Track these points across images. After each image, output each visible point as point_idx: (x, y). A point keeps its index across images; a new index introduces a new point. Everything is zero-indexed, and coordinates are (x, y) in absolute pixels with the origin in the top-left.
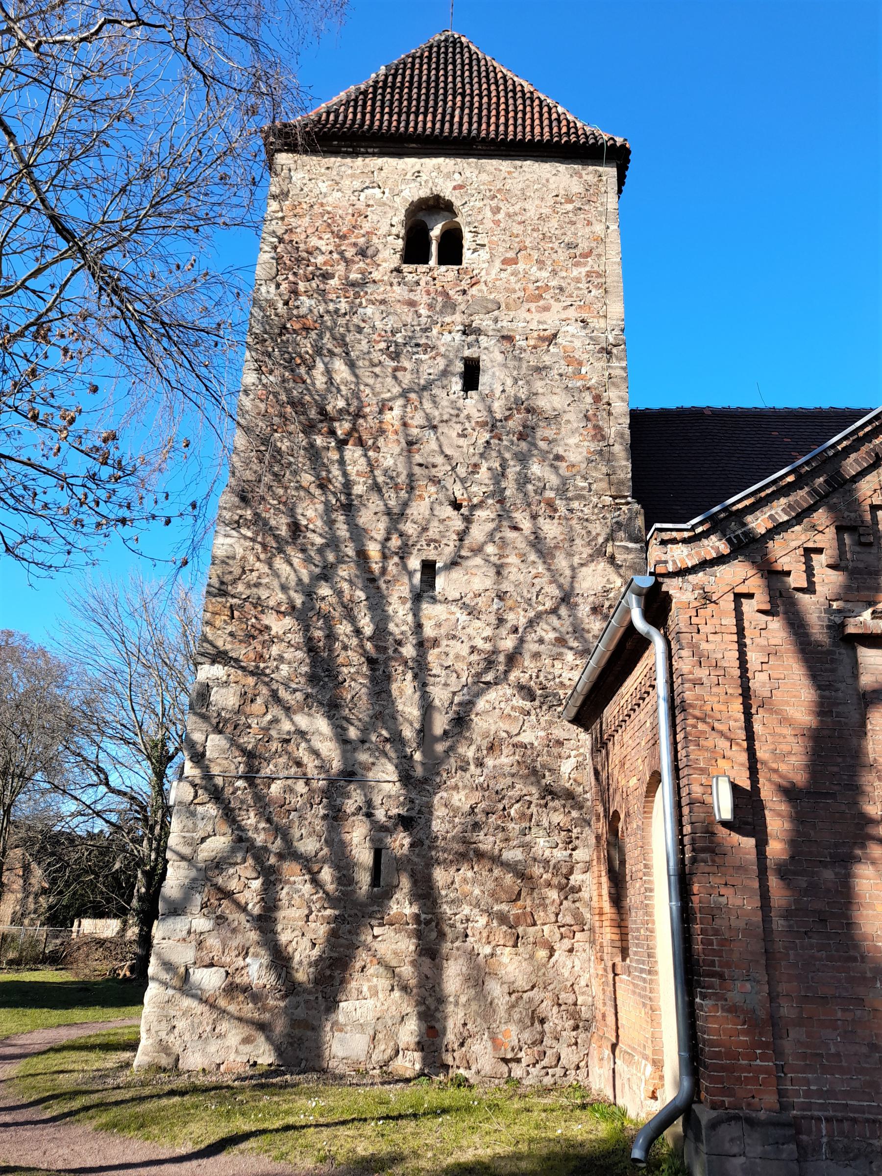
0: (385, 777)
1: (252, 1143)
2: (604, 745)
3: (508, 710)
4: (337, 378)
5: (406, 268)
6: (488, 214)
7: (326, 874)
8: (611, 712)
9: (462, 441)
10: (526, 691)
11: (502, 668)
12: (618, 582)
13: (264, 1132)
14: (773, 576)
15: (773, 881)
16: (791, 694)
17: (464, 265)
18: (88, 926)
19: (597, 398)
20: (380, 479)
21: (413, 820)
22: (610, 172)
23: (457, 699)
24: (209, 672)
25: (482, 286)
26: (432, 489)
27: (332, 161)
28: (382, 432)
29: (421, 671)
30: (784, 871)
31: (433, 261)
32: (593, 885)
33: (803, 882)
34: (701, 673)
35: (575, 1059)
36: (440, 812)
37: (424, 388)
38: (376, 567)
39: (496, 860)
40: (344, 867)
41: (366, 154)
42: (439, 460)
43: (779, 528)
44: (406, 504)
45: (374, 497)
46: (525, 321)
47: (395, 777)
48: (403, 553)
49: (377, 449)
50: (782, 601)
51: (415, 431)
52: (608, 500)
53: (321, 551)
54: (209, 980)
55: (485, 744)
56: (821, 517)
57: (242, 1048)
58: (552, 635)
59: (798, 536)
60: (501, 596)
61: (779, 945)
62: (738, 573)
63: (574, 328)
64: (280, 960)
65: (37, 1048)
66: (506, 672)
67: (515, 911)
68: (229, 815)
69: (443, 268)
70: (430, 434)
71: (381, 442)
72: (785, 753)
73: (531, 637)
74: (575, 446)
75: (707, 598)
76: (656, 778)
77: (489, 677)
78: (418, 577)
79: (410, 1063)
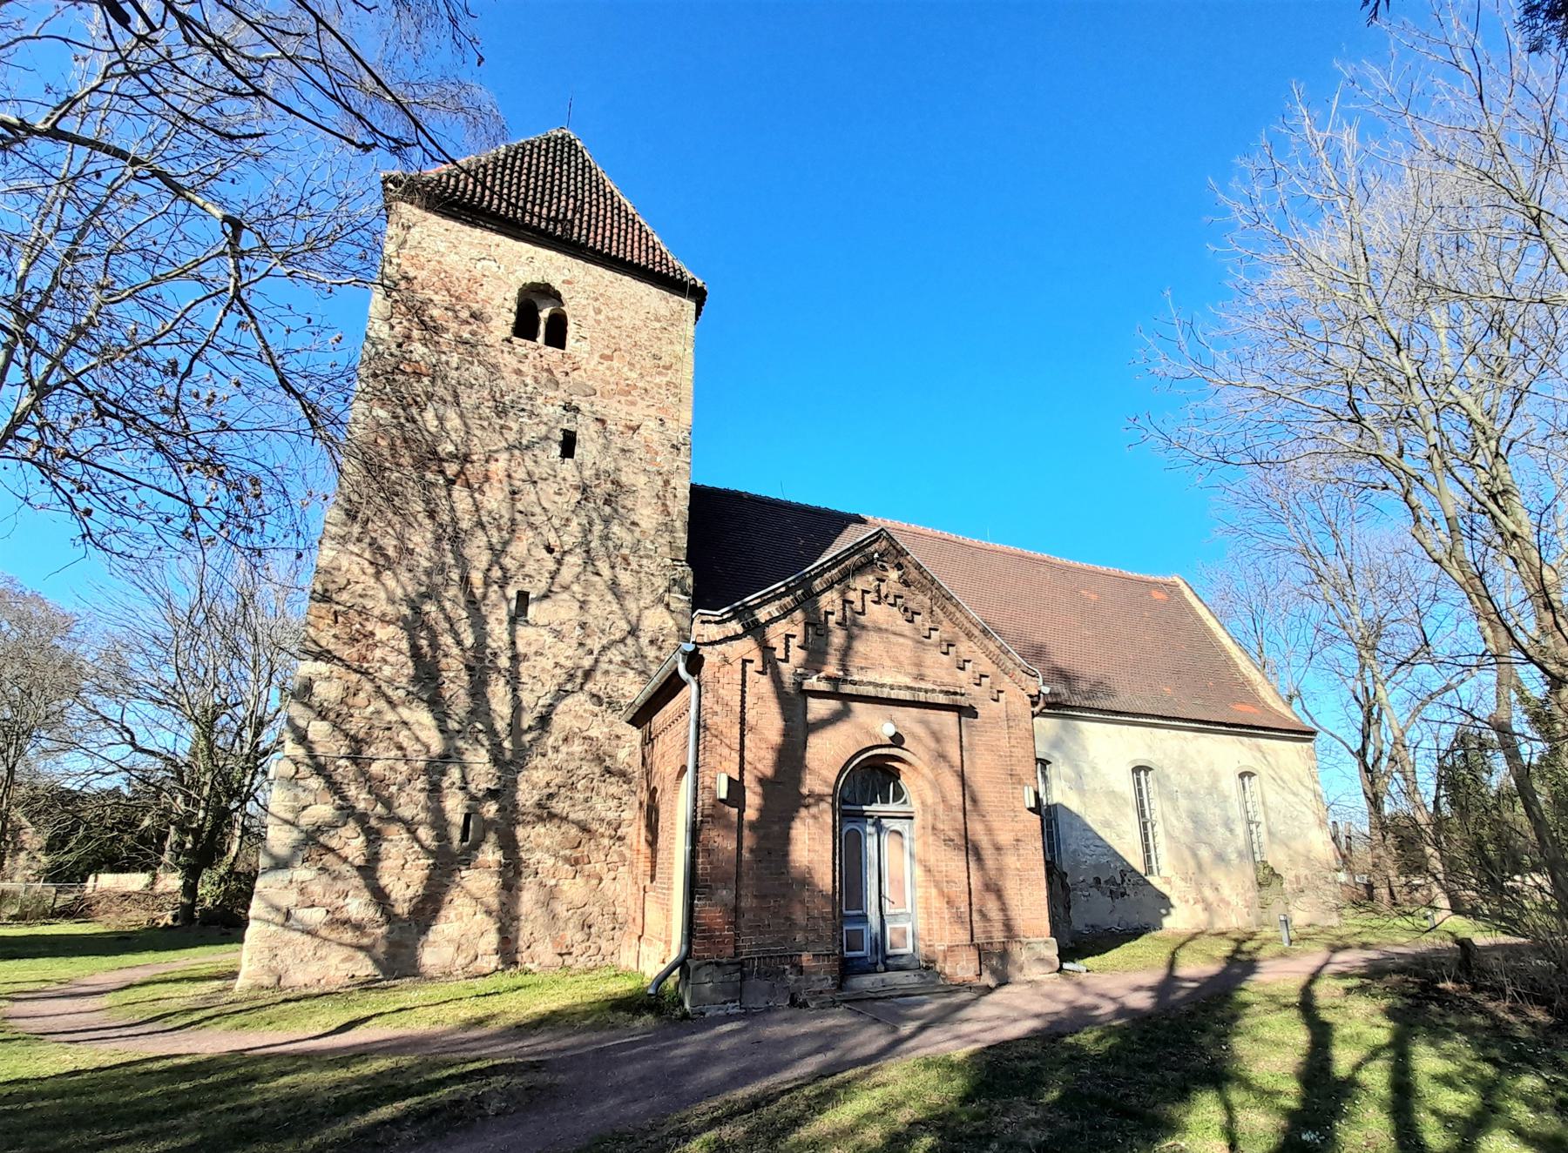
0: (479, 760)
1: (374, 1021)
2: (651, 740)
3: (581, 712)
4: (448, 425)
5: (514, 339)
6: (592, 313)
7: (424, 833)
8: (659, 719)
9: (557, 498)
10: (596, 698)
11: (579, 681)
12: (671, 623)
13: (381, 1014)
14: (766, 649)
15: (746, 832)
16: (769, 723)
17: (568, 350)
18: (107, 881)
19: (667, 483)
20: (484, 519)
21: (502, 793)
22: (691, 305)
23: (541, 702)
24: (308, 668)
25: (581, 372)
26: (531, 534)
27: (451, 224)
28: (487, 478)
29: (514, 681)
30: (753, 826)
31: (541, 339)
32: (635, 832)
33: (762, 832)
34: (717, 708)
35: (611, 949)
36: (523, 786)
37: (527, 447)
38: (478, 592)
39: (565, 819)
40: (439, 822)
41: (484, 227)
42: (538, 510)
43: (773, 620)
44: (506, 543)
45: (479, 533)
46: (616, 411)
47: (486, 759)
48: (504, 583)
49: (483, 493)
50: (770, 665)
51: (518, 483)
52: (669, 562)
53: (428, 573)
54: (316, 916)
55: (562, 735)
56: (798, 615)
57: (342, 966)
58: (619, 658)
59: (781, 628)
60: (583, 626)
61: (744, 868)
62: (747, 647)
63: (653, 424)
64: (380, 897)
65: (204, 973)
66: (582, 684)
67: (577, 854)
68: (334, 787)
69: (550, 349)
70: (528, 487)
71: (486, 487)
72: (762, 759)
73: (604, 659)
74: (647, 516)
75: (726, 660)
76: (684, 769)
77: (569, 687)
78: (514, 604)
79: (493, 961)
